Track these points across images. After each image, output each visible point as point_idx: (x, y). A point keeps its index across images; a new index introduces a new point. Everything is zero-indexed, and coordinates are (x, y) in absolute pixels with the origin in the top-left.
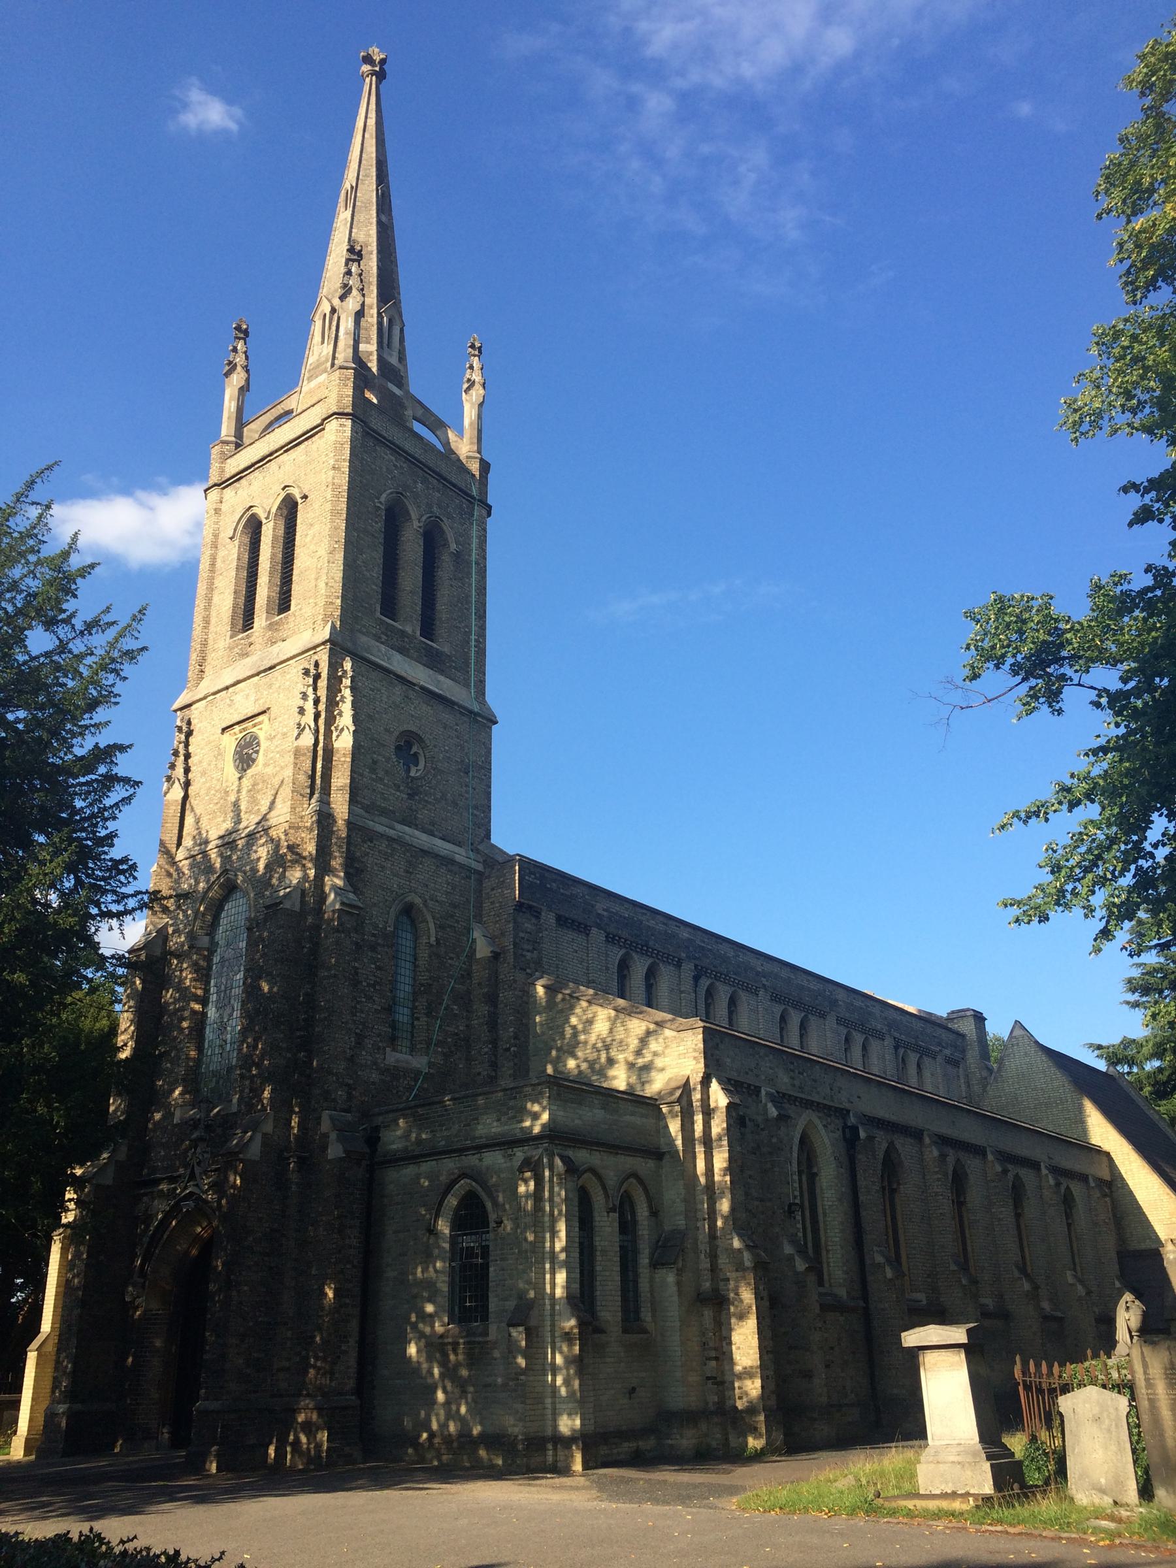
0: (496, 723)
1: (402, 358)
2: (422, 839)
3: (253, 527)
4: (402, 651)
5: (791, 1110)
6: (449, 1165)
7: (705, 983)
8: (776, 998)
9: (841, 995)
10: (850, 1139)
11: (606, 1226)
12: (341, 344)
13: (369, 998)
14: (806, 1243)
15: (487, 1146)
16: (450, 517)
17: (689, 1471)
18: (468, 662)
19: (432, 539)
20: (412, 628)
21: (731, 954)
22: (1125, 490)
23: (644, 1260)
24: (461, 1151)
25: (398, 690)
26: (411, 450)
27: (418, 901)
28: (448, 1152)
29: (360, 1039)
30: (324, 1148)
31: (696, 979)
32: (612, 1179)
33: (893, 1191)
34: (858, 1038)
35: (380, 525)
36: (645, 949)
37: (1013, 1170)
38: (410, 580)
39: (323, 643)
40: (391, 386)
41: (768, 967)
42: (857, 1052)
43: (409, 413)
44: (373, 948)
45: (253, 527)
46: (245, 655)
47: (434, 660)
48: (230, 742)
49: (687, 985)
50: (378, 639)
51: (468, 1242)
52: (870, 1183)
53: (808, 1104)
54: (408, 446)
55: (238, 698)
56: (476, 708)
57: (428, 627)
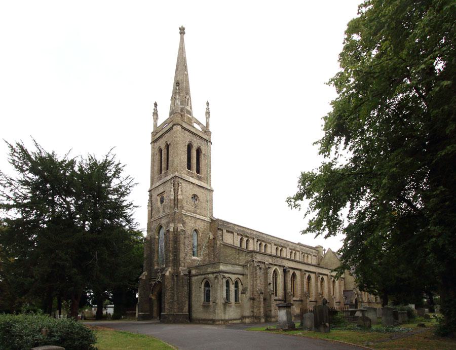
0: (213, 191)
1: (191, 108)
2: (198, 216)
3: (161, 151)
4: (192, 177)
5: (271, 266)
6: (203, 276)
7: (259, 242)
8: (275, 245)
9: (290, 244)
10: (285, 271)
11: (232, 287)
12: (163, 163)
13: (188, 247)
14: (273, 290)
15: (210, 273)
16: (202, 146)
17: (204, 296)
18: (208, 179)
19: (199, 151)
20: (195, 171)
21: (265, 236)
22: (313, 145)
23: (240, 293)
24: (205, 274)
25: (192, 185)
26: (193, 131)
27: (197, 228)
28: (202, 275)
29: (186, 255)
30: (180, 274)
31: (257, 242)
32: (233, 279)
33: (309, 282)
34: (294, 252)
35: (186, 149)
36: (246, 236)
37: (321, 276)
38: (194, 161)
39: (207, 123)
40: (188, 115)
41: (274, 239)
42: (293, 254)
43: (193, 121)
44: (188, 238)
45: (161, 151)
46: (160, 179)
47: (199, 179)
48: (159, 198)
49: (255, 243)
50: (187, 175)
51: (207, 289)
52: (305, 281)
53: (276, 265)
54: (192, 130)
55: (160, 189)
56: (209, 188)
57: (198, 171)
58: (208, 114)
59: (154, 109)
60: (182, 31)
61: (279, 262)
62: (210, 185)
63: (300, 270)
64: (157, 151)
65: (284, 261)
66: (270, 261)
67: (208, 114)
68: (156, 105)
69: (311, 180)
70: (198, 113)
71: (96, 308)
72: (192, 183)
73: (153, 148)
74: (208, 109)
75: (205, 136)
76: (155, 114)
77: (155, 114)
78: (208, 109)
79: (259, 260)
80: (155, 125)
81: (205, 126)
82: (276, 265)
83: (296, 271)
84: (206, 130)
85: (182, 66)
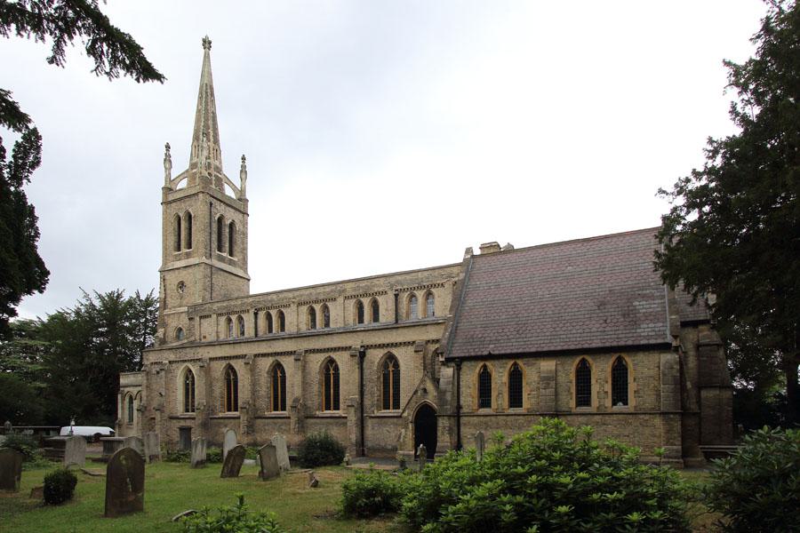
1: (220, 163)
10: (206, 369)
18: (244, 264)
53: (185, 361)
58: (243, 171)
59: (166, 154)
60: (207, 44)
61: (190, 354)
62: (245, 270)
63: (243, 357)
64: (173, 220)
65: (199, 350)
66: (172, 357)
67: (243, 171)
68: (244, 159)
69: (33, 237)
70: (230, 169)
71: (105, 479)
72: (195, 265)
73: (165, 212)
74: (244, 167)
75: (240, 206)
76: (168, 159)
77: (168, 159)
78: (244, 167)
79: (153, 361)
80: (168, 176)
81: (172, 179)
82: (185, 361)
83: (233, 363)
84: (243, 200)
85: (207, 94)
